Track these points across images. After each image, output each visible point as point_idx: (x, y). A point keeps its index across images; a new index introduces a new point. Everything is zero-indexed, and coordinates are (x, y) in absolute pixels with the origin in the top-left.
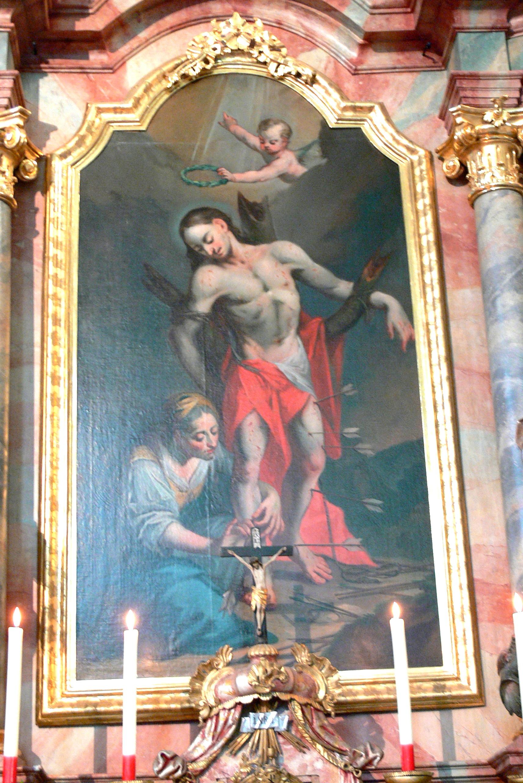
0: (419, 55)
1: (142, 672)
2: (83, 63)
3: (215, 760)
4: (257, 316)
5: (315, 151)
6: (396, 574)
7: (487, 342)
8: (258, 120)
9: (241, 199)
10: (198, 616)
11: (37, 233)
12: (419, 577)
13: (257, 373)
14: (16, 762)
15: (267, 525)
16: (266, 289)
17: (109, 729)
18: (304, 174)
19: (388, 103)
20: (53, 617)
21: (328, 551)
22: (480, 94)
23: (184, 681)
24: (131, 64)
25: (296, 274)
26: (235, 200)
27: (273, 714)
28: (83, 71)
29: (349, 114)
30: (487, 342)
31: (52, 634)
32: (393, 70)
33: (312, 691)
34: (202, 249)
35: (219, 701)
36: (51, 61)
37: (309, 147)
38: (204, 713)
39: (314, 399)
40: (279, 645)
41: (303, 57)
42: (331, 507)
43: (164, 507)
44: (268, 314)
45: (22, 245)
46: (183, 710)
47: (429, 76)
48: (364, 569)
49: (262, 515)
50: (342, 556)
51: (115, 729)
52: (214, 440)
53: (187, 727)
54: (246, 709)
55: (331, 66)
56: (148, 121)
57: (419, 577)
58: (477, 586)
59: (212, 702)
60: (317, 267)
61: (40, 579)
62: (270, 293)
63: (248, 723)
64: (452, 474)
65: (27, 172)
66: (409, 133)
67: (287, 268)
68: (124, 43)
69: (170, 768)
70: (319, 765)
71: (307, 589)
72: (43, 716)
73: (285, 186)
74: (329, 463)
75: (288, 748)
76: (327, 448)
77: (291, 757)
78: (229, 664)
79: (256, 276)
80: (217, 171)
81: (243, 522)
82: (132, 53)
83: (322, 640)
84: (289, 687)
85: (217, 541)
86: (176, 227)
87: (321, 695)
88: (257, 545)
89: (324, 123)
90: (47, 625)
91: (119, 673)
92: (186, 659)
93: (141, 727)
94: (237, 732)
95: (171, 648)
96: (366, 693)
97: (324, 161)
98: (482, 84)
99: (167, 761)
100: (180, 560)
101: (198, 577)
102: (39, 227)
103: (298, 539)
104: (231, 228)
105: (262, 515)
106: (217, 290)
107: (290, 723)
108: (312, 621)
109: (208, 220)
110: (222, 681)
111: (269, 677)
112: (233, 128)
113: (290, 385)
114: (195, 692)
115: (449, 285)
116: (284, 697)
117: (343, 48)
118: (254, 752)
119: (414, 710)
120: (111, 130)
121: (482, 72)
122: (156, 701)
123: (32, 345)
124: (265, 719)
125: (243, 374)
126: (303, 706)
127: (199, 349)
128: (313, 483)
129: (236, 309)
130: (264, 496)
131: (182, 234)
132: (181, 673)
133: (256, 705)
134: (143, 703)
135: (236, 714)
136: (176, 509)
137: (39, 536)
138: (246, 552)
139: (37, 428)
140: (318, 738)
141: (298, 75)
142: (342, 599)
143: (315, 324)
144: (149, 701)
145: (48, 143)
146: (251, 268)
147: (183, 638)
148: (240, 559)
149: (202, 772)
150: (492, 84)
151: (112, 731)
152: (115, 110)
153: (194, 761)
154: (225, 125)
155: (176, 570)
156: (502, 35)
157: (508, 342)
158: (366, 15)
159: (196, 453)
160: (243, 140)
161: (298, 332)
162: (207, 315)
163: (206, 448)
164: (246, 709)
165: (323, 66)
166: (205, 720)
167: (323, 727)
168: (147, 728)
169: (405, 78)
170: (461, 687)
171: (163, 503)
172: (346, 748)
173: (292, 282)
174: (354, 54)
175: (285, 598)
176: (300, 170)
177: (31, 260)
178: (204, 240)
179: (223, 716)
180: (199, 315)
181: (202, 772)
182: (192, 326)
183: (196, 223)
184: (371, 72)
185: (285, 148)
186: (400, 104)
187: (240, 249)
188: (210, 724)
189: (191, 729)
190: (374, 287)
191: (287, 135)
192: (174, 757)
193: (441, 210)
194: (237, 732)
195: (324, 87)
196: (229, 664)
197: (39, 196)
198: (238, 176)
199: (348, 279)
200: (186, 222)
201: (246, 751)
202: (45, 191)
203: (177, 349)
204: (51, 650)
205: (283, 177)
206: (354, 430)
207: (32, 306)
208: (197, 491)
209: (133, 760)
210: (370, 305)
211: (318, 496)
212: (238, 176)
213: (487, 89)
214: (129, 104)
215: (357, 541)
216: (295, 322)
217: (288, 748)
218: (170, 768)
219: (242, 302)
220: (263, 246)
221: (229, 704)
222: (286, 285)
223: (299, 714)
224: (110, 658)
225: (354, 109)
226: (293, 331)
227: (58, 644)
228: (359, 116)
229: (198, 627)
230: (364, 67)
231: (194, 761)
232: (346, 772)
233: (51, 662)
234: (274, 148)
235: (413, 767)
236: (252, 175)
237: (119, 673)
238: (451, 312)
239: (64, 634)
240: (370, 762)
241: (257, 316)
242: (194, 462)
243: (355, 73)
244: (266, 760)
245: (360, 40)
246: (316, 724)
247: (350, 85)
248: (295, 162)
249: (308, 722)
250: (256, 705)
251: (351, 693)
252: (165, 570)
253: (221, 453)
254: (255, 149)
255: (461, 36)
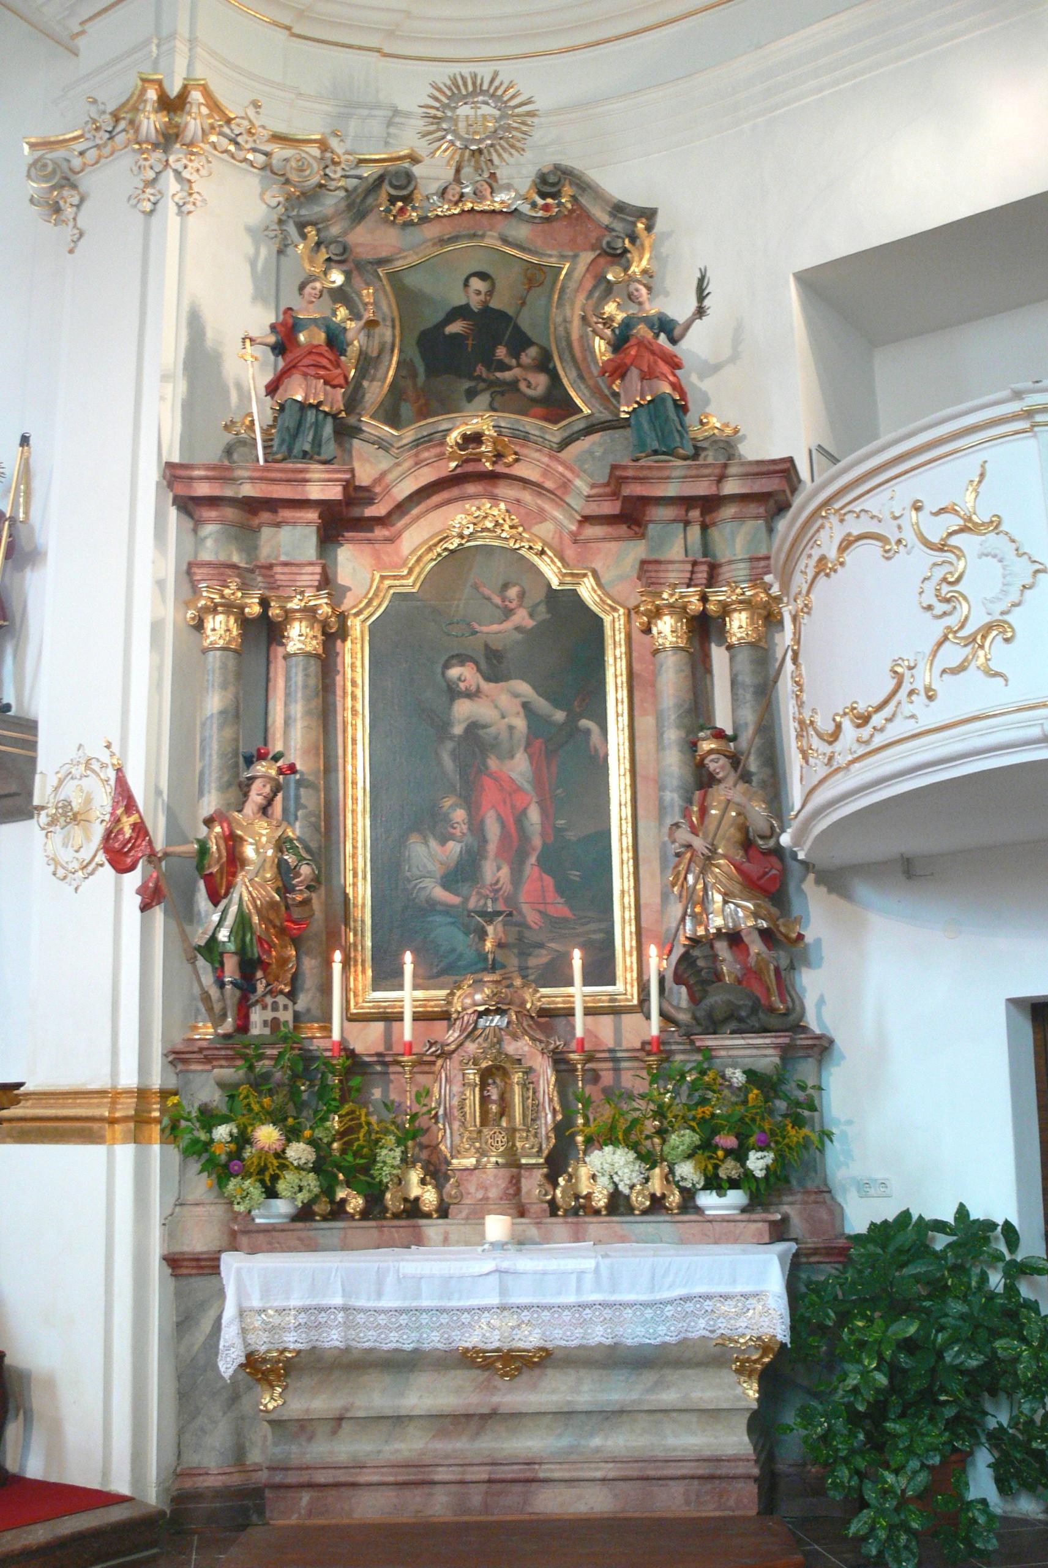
0: (624, 527)
1: (416, 987)
2: (369, 535)
3: (461, 1044)
4: (496, 738)
5: (542, 608)
6: (588, 923)
7: (658, 761)
8: (501, 582)
9: (487, 646)
10: (453, 950)
11: (339, 672)
12: (603, 926)
13: (496, 780)
14: (340, 1043)
15: (501, 889)
16: (503, 717)
17: (624, 1016)
18: (533, 628)
19: (598, 565)
20: (356, 950)
21: (541, 907)
22: (662, 575)
23: (443, 993)
24: (406, 535)
25: (525, 706)
26: (482, 648)
27: (498, 1017)
28: (370, 541)
29: (568, 579)
30: (658, 761)
31: (356, 961)
32: (604, 539)
33: (523, 1003)
34: (458, 686)
35: (464, 1009)
36: (346, 534)
37: (538, 604)
38: (454, 1016)
39: (535, 799)
40: (506, 970)
41: (536, 529)
42: (545, 877)
43: (429, 875)
44: (504, 736)
45: (327, 681)
46: (442, 1012)
47: (632, 543)
48: (566, 920)
49: (497, 882)
50: (551, 910)
51: (398, 1023)
52: (465, 828)
53: (445, 1023)
54: (481, 1014)
55: (557, 536)
56: (418, 585)
57: (603, 926)
58: (644, 932)
59: (460, 1009)
60: (541, 699)
61: (347, 924)
62: (506, 720)
63: (482, 1022)
64: (628, 855)
65: (331, 628)
66: (613, 592)
67: (518, 701)
68: (401, 518)
69: (433, 1049)
70: (526, 1048)
71: (527, 934)
72: (352, 1014)
73: (519, 636)
74: (544, 844)
75: (507, 1038)
76: (543, 835)
77: (509, 1043)
78: (470, 986)
79: (496, 707)
80: (469, 624)
81: (484, 886)
82: (407, 526)
83: (537, 967)
84: (507, 1001)
85: (466, 900)
86: (439, 670)
87: (528, 1006)
88: (490, 910)
89: (549, 585)
90: (352, 955)
91: (401, 987)
92: (444, 979)
93: (589, 1018)
94: (475, 1028)
95: (435, 971)
96: (564, 1002)
97: (548, 616)
98: (663, 567)
99: (431, 1045)
100: (441, 913)
101: (453, 923)
102: (340, 668)
103: (522, 898)
104: (479, 670)
105: (497, 882)
106: (468, 718)
107: (509, 1023)
108: (529, 955)
109: (462, 664)
110: (466, 997)
111: (494, 995)
112: (482, 589)
113: (519, 789)
114: (450, 1003)
115: (636, 713)
116: (505, 1007)
117: (566, 522)
118: (486, 1040)
119: (585, 1014)
120: (392, 591)
121: (662, 559)
122: (425, 1006)
123: (337, 757)
124: (492, 1021)
125: (487, 781)
126: (517, 1013)
127: (454, 761)
128: (533, 859)
129: (481, 732)
130: (499, 869)
131: (443, 674)
132: (441, 988)
133: (487, 1012)
134: (416, 1007)
135: (474, 1017)
136: (438, 876)
137: (346, 895)
138: (483, 914)
139: (342, 818)
140: (526, 1033)
141: (531, 548)
142: (552, 940)
143: (539, 743)
144: (420, 1006)
145: (346, 601)
146: (493, 701)
147: (442, 965)
148: (479, 919)
149: (454, 1051)
150: (671, 567)
151: (395, 1025)
152: (395, 577)
153: (448, 1045)
154: (476, 587)
155: (439, 919)
156: (682, 525)
157: (670, 766)
158: (582, 502)
159: (452, 838)
160: (489, 599)
161: (526, 750)
162: (460, 736)
163: (459, 834)
164: (481, 1014)
165: (551, 535)
166: (456, 1020)
167: (529, 1026)
168: (419, 1023)
169: (613, 546)
170: (627, 1000)
171: (429, 872)
172: (543, 1038)
173: (521, 710)
174: (574, 528)
175: (511, 940)
176: (530, 623)
177: (334, 693)
178: (459, 679)
179: (466, 1018)
180: (455, 737)
181: (454, 1051)
182: (450, 745)
183: (453, 666)
184: (588, 541)
185: (520, 606)
186: (608, 567)
187: (485, 686)
188: (458, 1023)
189: (843, 1226)
190: (581, 716)
191: (522, 595)
192: (436, 1043)
193: (635, 654)
194: (475, 1028)
195: (550, 557)
196: (470, 986)
197: (339, 642)
198: (485, 629)
199: (562, 710)
200: (447, 666)
201: (480, 1040)
202: (344, 640)
203: (440, 763)
204: (356, 971)
205: (518, 629)
206: (563, 822)
207: (336, 728)
208: (452, 865)
209: (410, 1044)
210: (578, 729)
211: (536, 869)
212: (485, 629)
213: (667, 571)
214: (405, 572)
215: (562, 900)
216: (523, 743)
217: (507, 1038)
218: (433, 1049)
219: (484, 727)
220: (501, 684)
221: (469, 1011)
222: (518, 713)
223: (514, 1017)
224: (395, 977)
225: (572, 575)
226: (522, 749)
227: (360, 968)
228: (576, 580)
229: (452, 957)
230: (582, 538)
231: (448, 1045)
232: (543, 1053)
233: (355, 979)
234: (512, 606)
235: (583, 1051)
236: (495, 627)
237: (401, 987)
238: (637, 734)
239: (363, 961)
240: (557, 1048)
241: (496, 738)
242: (451, 844)
243: (575, 542)
244: (493, 1045)
245: (579, 518)
246: (525, 1024)
247: (570, 552)
248: (527, 617)
249: (520, 1023)
250: (487, 1012)
251: (554, 1002)
252: (431, 919)
253: (469, 839)
254: (497, 607)
255: (651, 526)
